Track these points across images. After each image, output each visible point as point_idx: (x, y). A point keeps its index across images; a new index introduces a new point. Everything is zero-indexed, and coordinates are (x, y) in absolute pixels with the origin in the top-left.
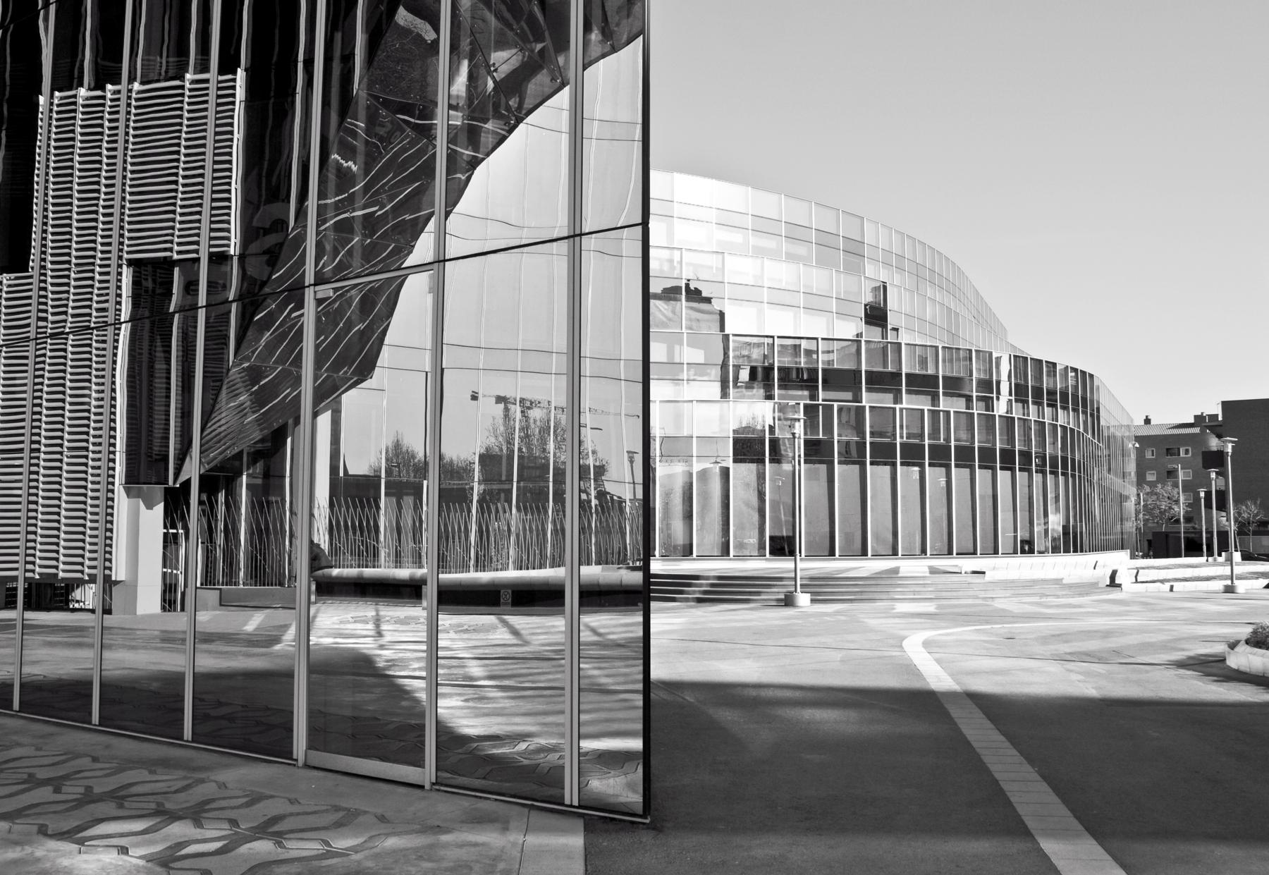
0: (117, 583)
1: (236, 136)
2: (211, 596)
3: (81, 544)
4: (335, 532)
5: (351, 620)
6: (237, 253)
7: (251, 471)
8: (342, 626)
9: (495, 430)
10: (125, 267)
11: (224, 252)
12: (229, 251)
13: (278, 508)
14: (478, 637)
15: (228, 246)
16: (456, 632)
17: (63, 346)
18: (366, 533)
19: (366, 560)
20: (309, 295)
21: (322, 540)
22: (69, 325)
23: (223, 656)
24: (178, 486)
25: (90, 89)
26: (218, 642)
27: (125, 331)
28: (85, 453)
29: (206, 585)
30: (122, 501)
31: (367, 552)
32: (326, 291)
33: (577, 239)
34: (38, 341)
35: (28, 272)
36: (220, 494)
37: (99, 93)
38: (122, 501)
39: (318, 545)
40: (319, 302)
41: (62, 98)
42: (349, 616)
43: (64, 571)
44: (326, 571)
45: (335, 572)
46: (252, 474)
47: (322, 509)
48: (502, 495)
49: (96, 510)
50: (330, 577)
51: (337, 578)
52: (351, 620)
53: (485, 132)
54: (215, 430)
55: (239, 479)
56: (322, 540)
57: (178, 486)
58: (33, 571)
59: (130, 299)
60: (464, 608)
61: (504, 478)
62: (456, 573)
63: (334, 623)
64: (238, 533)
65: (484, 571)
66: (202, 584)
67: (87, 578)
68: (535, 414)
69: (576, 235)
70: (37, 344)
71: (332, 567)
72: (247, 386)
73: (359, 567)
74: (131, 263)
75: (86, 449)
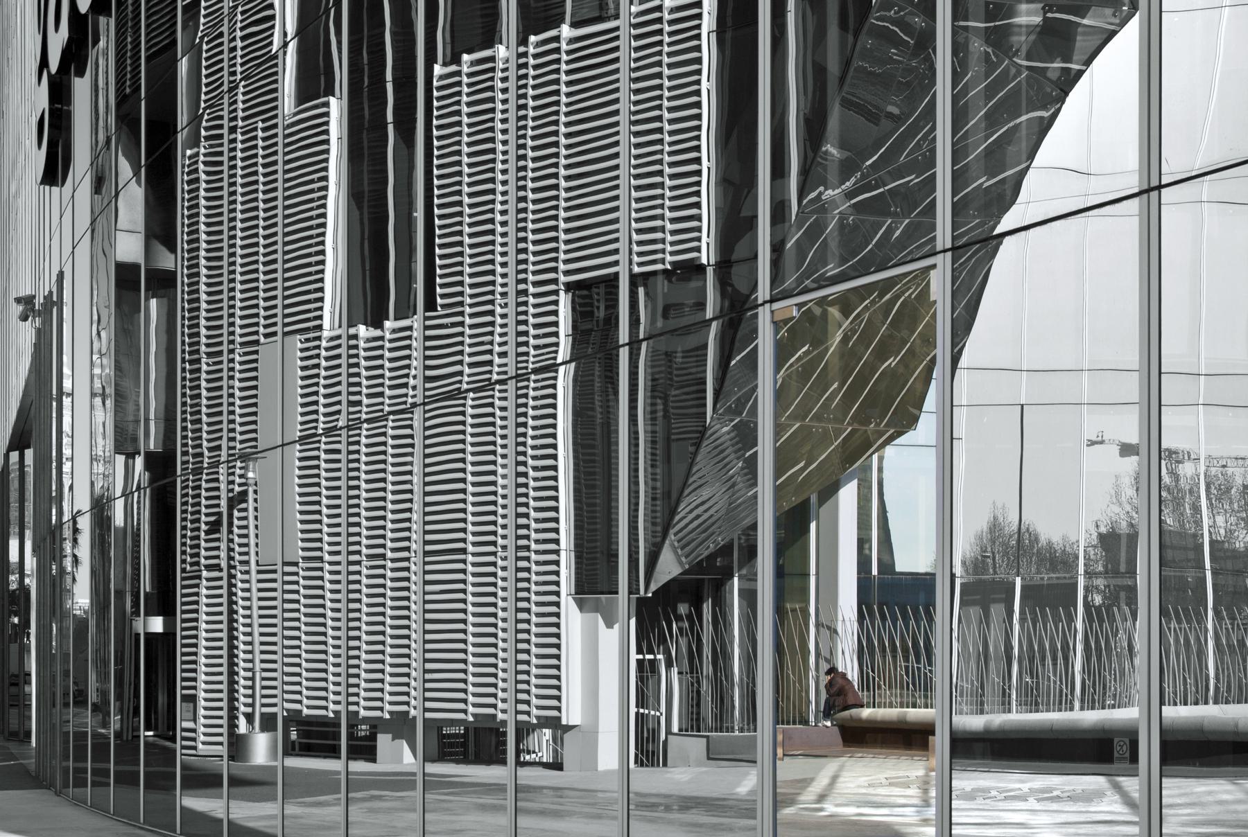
0: (569, 728)
1: (705, 85)
2: (696, 746)
3: (462, 676)
4: (866, 656)
5: (884, 781)
6: (712, 261)
7: (744, 572)
8: (871, 791)
9: (1118, 494)
10: (562, 293)
11: (692, 260)
12: (699, 258)
13: (796, 618)
14: (1074, 809)
15: (698, 249)
16: (1038, 800)
17: (461, 409)
18: (912, 657)
19: (913, 696)
20: (764, 318)
21: (849, 666)
22: (466, 379)
23: (698, 829)
24: (650, 595)
25: (445, 64)
26: (694, 811)
27: (564, 380)
28: (382, 563)
29: (692, 731)
30: (572, 619)
31: (914, 685)
32: (789, 307)
33: (1154, 194)
34: (427, 408)
35: (437, 311)
36: (705, 605)
37: (454, 68)
38: (572, 619)
39: (844, 675)
40: (777, 325)
41: (473, 64)
42: (881, 777)
43: (365, 708)
44: (854, 711)
45: (866, 713)
46: (746, 575)
47: (848, 623)
48: (1123, 595)
49: (337, 633)
50: (860, 720)
51: (869, 721)
52: (884, 781)
53: (1084, 34)
54: (698, 517)
55: (729, 583)
56: (849, 666)
57: (650, 595)
58: (528, 713)
59: (571, 338)
60: (1060, 764)
61: (1123, 568)
62: (1048, 711)
63: (859, 787)
64: (731, 658)
65: (1093, 708)
66: (680, 730)
67: (535, 721)
68: (1186, 469)
69: (1151, 189)
70: (425, 412)
71: (862, 706)
72: (739, 450)
73: (902, 706)
74: (569, 287)
75: (464, 551)
